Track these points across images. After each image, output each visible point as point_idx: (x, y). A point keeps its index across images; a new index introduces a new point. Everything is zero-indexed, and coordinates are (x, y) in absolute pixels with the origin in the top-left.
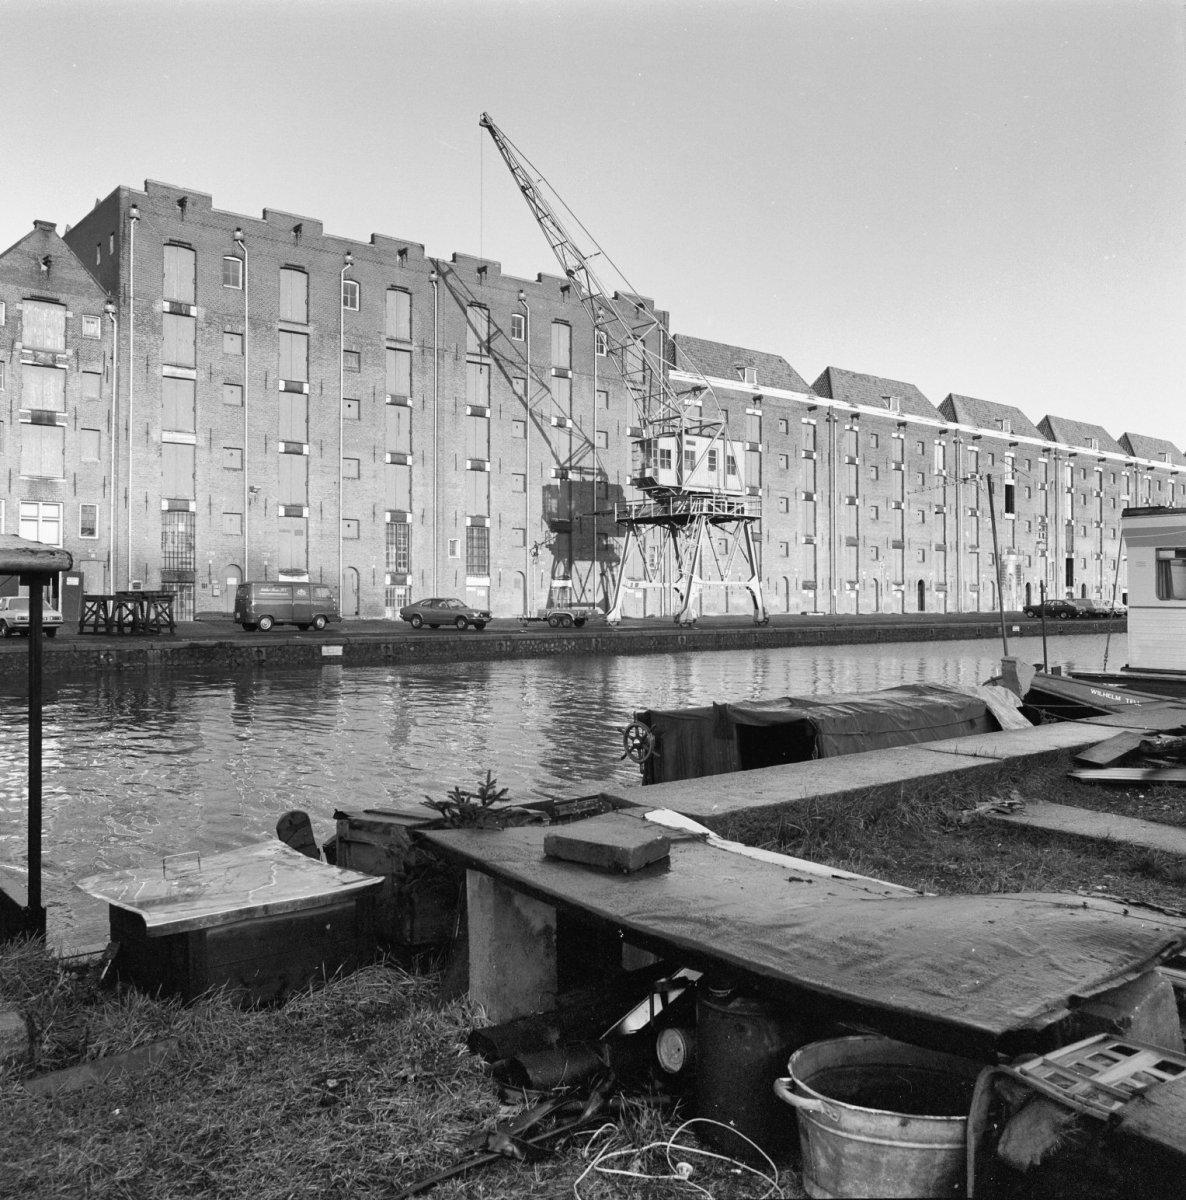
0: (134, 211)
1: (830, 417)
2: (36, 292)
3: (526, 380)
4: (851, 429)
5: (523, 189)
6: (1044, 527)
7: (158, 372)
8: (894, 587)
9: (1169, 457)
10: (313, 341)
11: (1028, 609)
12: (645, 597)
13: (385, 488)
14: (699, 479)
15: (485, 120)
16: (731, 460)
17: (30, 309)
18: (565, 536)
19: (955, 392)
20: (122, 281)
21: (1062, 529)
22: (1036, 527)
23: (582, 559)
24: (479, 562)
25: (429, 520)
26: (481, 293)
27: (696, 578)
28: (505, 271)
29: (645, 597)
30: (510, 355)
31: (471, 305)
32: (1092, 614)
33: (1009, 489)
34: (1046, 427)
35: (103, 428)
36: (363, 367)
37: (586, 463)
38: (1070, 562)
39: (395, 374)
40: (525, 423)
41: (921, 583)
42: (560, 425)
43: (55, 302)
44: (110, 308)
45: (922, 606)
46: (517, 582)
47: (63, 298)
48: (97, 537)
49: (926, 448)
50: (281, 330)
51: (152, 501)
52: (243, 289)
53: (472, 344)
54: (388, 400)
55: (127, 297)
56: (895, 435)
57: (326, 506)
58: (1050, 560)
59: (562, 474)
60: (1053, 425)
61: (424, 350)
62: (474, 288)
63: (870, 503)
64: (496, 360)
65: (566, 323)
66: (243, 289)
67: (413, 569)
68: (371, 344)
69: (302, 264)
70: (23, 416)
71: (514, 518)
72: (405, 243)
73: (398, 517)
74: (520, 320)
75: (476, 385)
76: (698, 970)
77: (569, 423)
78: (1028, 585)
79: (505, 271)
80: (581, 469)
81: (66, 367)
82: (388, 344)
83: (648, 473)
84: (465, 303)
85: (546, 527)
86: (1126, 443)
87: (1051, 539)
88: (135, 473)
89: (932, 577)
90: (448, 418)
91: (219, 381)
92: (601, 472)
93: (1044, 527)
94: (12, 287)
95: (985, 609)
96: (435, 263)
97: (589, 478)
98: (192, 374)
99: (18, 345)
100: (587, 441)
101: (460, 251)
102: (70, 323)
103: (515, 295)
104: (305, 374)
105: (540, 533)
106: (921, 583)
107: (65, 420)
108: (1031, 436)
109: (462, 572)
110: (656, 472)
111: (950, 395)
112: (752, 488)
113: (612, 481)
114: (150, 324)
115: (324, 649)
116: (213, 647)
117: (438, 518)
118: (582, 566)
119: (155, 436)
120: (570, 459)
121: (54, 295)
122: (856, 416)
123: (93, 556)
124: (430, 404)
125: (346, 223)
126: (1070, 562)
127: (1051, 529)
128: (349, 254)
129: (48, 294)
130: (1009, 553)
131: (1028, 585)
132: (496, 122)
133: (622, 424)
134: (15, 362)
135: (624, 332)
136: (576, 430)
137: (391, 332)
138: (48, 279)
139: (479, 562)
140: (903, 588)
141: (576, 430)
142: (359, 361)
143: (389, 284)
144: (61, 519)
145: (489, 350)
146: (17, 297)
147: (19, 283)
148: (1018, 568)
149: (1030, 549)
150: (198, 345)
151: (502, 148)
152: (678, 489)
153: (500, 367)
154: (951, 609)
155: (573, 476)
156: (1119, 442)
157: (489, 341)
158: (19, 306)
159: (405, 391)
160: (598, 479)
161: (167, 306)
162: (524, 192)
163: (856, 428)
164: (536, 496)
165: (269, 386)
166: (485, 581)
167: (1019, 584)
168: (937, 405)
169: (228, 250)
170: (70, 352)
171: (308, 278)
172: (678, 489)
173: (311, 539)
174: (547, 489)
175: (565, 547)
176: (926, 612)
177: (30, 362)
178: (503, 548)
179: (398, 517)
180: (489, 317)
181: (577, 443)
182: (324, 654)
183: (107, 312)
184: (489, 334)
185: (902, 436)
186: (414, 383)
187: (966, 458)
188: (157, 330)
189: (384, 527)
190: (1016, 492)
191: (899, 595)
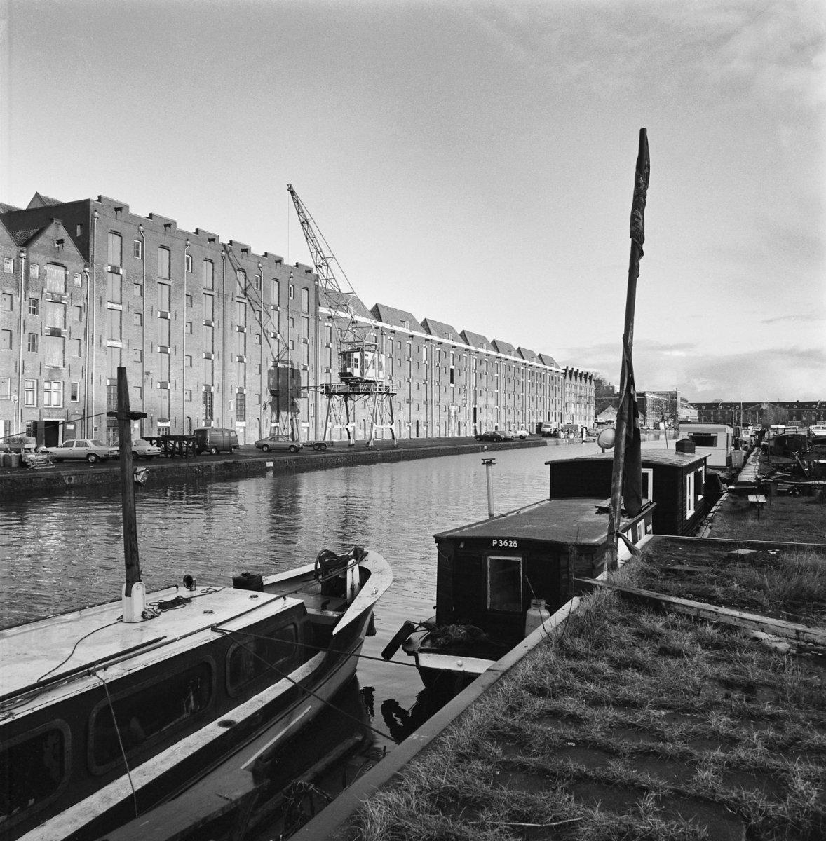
0: (96, 214)
1: (383, 332)
2: (53, 260)
3: (261, 312)
4: (390, 339)
5: (302, 223)
6: (465, 391)
7: (105, 305)
8: (407, 424)
9: (407, 323)
10: (172, 290)
11: (477, 437)
12: (308, 432)
13: (200, 374)
14: (370, 374)
15: (290, 188)
16: (381, 364)
17: (49, 268)
18: (276, 398)
19: (380, 302)
20: (91, 254)
21: (472, 392)
22: (462, 391)
23: (284, 411)
24: (242, 415)
25: (221, 390)
26: (244, 263)
27: (374, 424)
28: (132, 211)
29: (308, 432)
30: (255, 298)
31: (239, 269)
32: (507, 439)
33: (452, 370)
34: (376, 312)
35: (82, 338)
36: (194, 304)
37: (285, 358)
38: (475, 409)
39: (204, 308)
40: (260, 336)
41: (417, 422)
42: (275, 337)
43: (61, 265)
44: (87, 269)
45: (417, 436)
46: (256, 423)
47: (65, 263)
48: (78, 401)
49: (402, 345)
50: (204, 294)
51: (103, 380)
52: (142, 258)
53: (239, 292)
54: (204, 323)
55: (93, 261)
56: (408, 342)
57: (178, 383)
58: (468, 409)
59: (276, 366)
60: (429, 323)
61: (217, 294)
62: (240, 260)
63: (398, 379)
64: (249, 301)
65: (119, 234)
66: (142, 258)
67: (214, 417)
68: (197, 291)
69: (168, 245)
70: (47, 331)
71: (256, 389)
72: (214, 235)
73: (208, 388)
74: (257, 279)
75: (238, 313)
76: (690, 518)
77: (278, 336)
78: (459, 422)
79: (132, 211)
80: (283, 361)
81: (66, 303)
82: (204, 291)
83: (349, 370)
84: (237, 268)
85: (269, 394)
86: (425, 325)
87: (468, 397)
88: (96, 364)
89: (422, 419)
90: (229, 331)
91: (132, 311)
92: (292, 364)
93: (465, 391)
94: (43, 256)
95: (436, 435)
96: (224, 246)
97: (286, 366)
98: (120, 307)
99: (45, 290)
100: (286, 346)
101: (234, 239)
102: (68, 278)
103: (256, 264)
104: (168, 308)
105: (267, 398)
106: (417, 422)
107: (65, 334)
108: (363, 316)
109: (234, 418)
110: (353, 370)
111: (376, 305)
112: (390, 376)
113: (296, 368)
114: (102, 280)
115: (267, 463)
116: (231, 464)
117: (224, 389)
118: (283, 414)
119: (104, 343)
120: (278, 356)
121: (61, 262)
122: (394, 332)
123: (77, 412)
124: (221, 326)
125: (186, 224)
126: (475, 409)
127: (468, 392)
128: (188, 240)
129: (58, 261)
130: (452, 405)
131: (459, 422)
132: (295, 188)
133: (155, 309)
134: (44, 301)
135: (307, 286)
136: (281, 339)
137: (204, 285)
138: (59, 252)
139: (242, 415)
140: (410, 424)
141: (281, 339)
142: (191, 301)
143: (160, 244)
144: (62, 391)
145: (245, 294)
146: (45, 263)
147: (46, 254)
148: (455, 413)
149: (460, 403)
150: (123, 291)
151: (297, 202)
152: (361, 379)
153: (251, 304)
154: (429, 436)
155: (280, 365)
156: (421, 324)
157: (245, 290)
158: (45, 268)
159: (210, 318)
160: (290, 366)
161: (109, 268)
162: (302, 224)
163: (392, 338)
164: (265, 375)
165: (154, 314)
166: (243, 424)
167: (455, 422)
168: (420, 323)
169: (136, 236)
170: (68, 294)
171: (170, 253)
172: (361, 379)
173: (171, 401)
174: (270, 372)
175: (275, 404)
176: (420, 437)
177: (50, 300)
178: (252, 408)
179: (208, 388)
180: (245, 276)
181: (282, 346)
182: (267, 466)
183: (85, 272)
184: (245, 285)
185: (410, 343)
186: (215, 313)
187: (323, 331)
188: (105, 282)
189: (202, 394)
190: (455, 372)
191: (408, 428)
